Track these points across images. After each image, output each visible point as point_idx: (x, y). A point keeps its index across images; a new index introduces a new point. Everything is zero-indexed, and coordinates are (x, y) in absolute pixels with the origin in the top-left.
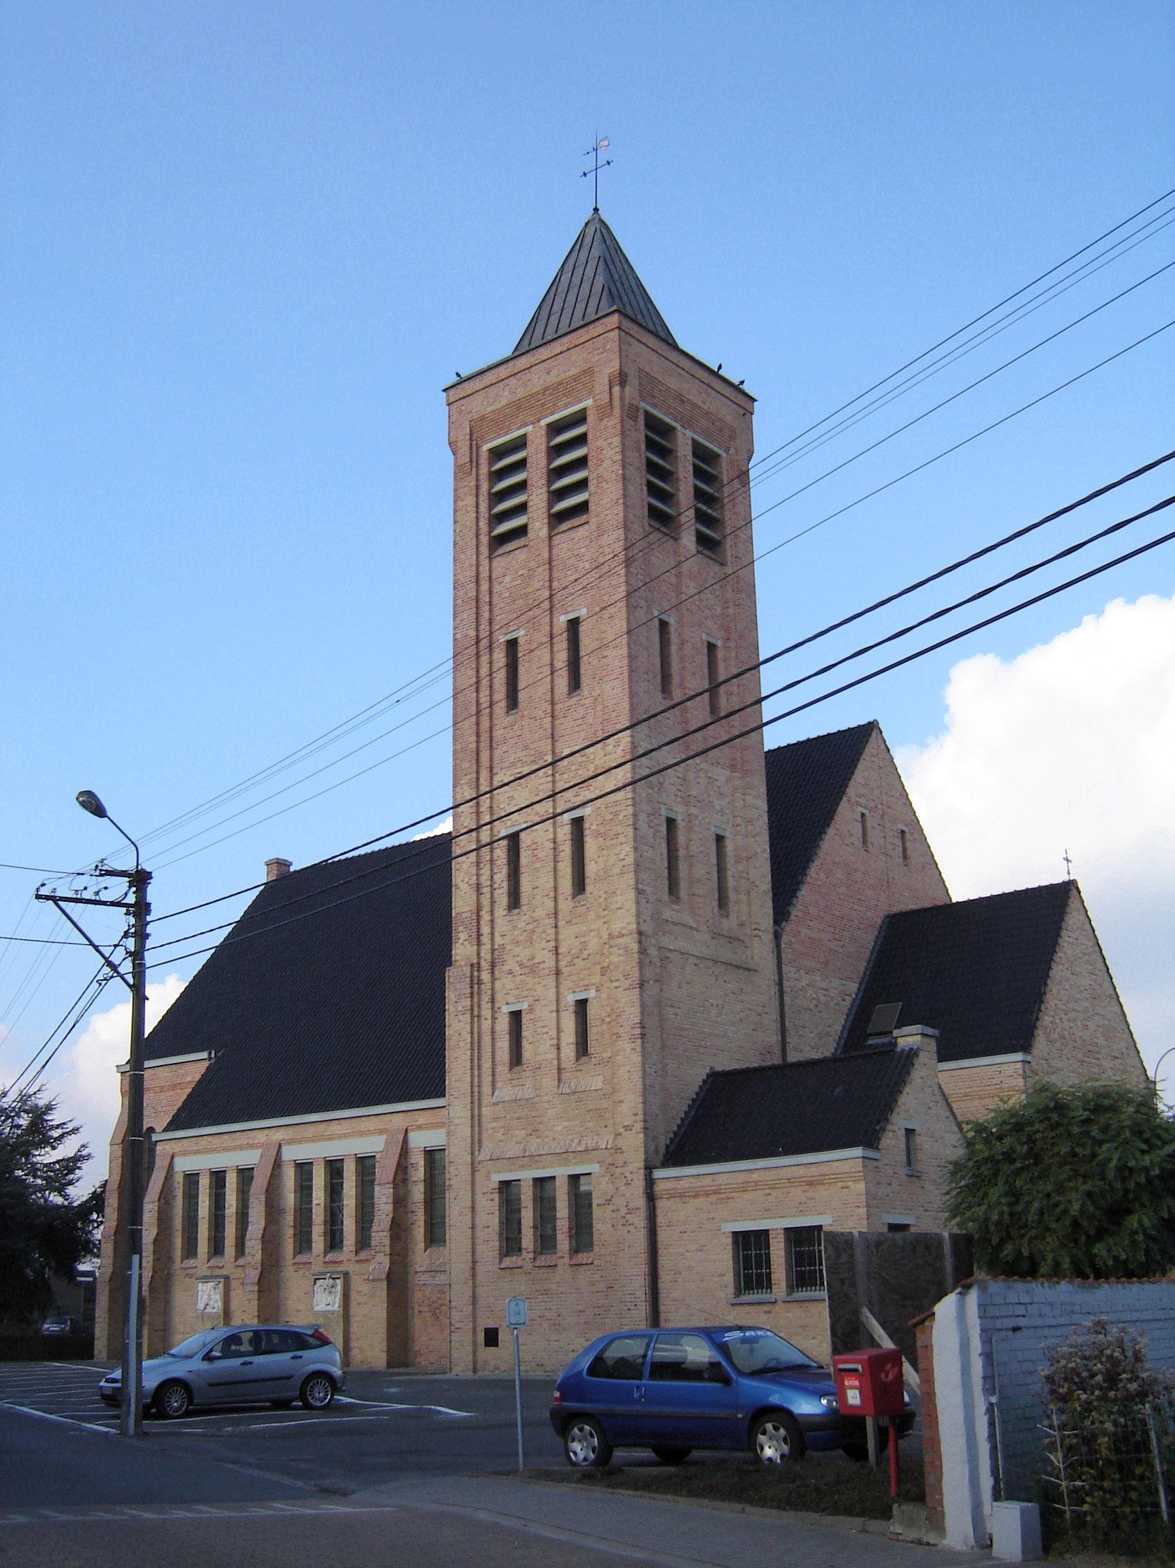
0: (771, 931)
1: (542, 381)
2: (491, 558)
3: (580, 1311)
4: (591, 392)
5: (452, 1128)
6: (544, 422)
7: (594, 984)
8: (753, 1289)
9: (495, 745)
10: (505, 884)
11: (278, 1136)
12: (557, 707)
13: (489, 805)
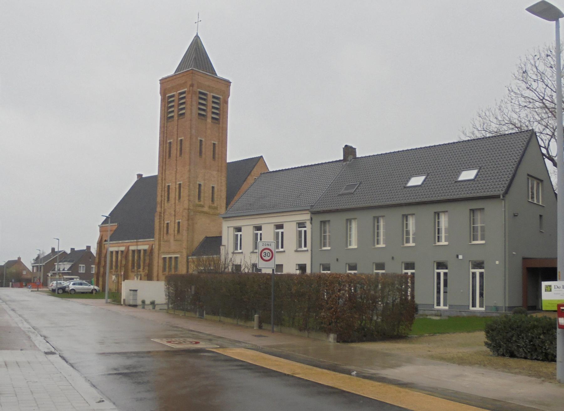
2: (167, 122)
11: (129, 244)
12: (178, 158)
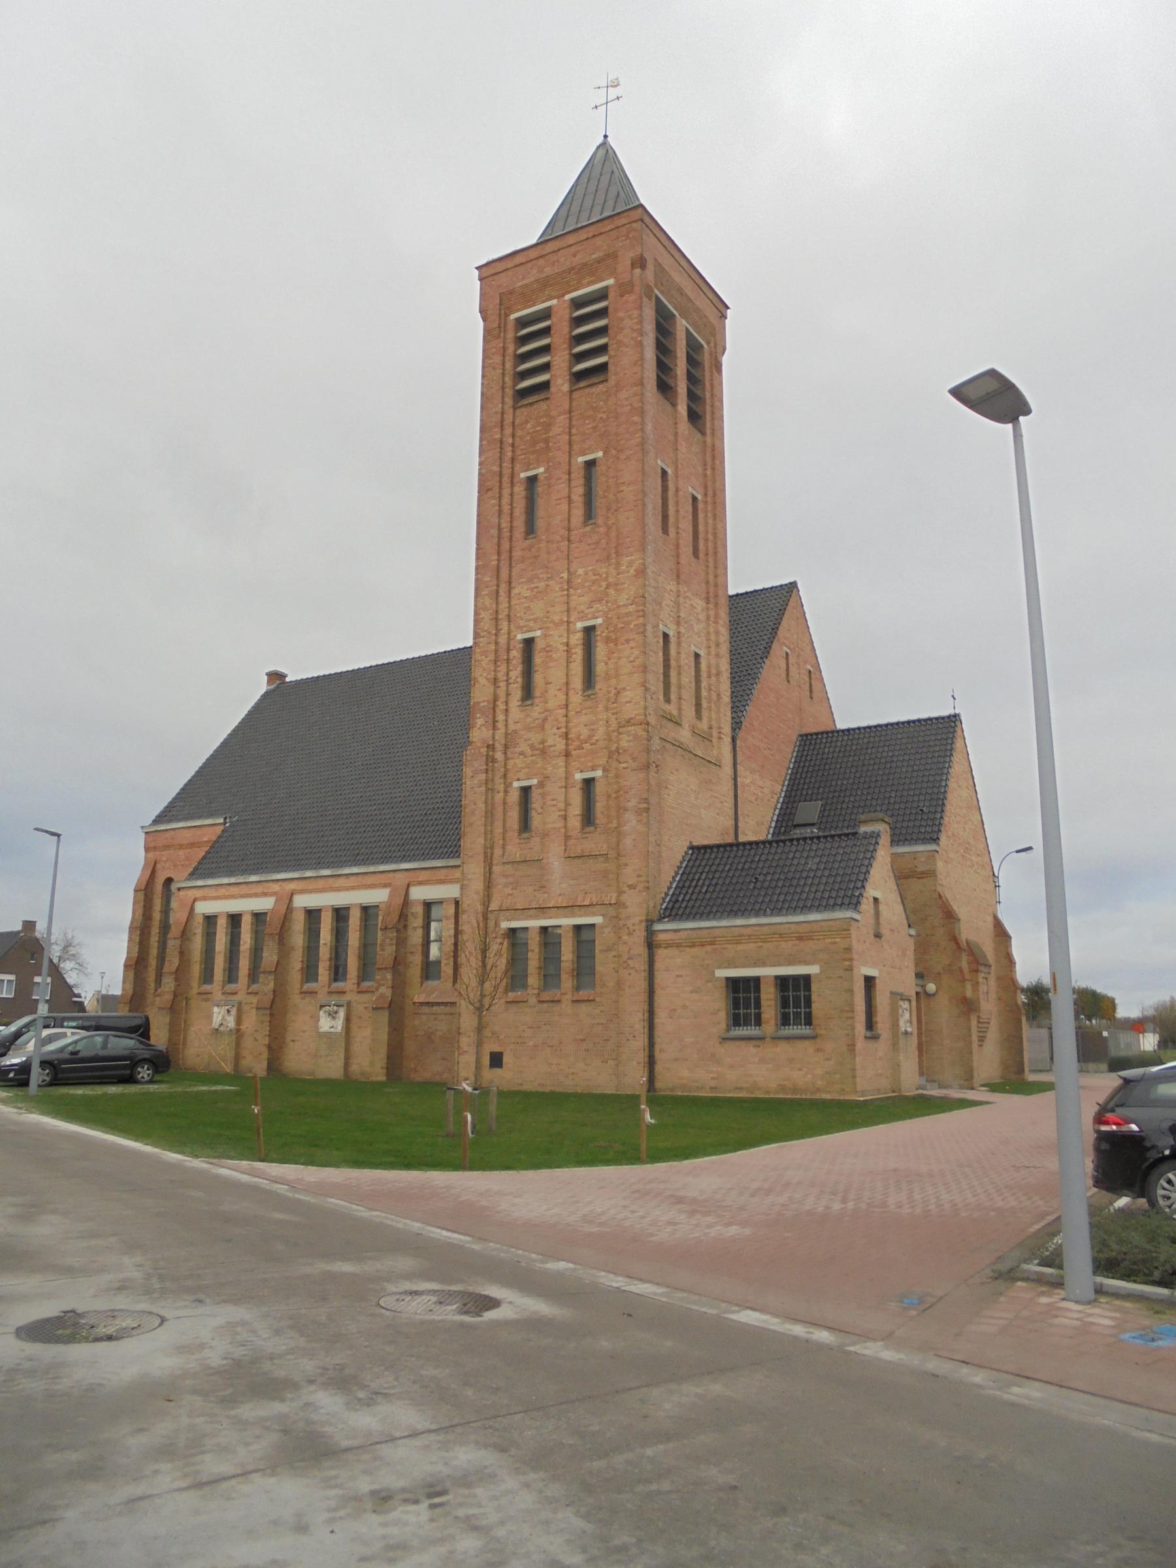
0: (730, 736)
1: (568, 263)
2: (515, 408)
3: (581, 1040)
4: (613, 273)
5: (466, 882)
6: (568, 297)
7: (601, 765)
8: (801, 1025)
9: (513, 564)
10: (520, 680)
13: (507, 613)
